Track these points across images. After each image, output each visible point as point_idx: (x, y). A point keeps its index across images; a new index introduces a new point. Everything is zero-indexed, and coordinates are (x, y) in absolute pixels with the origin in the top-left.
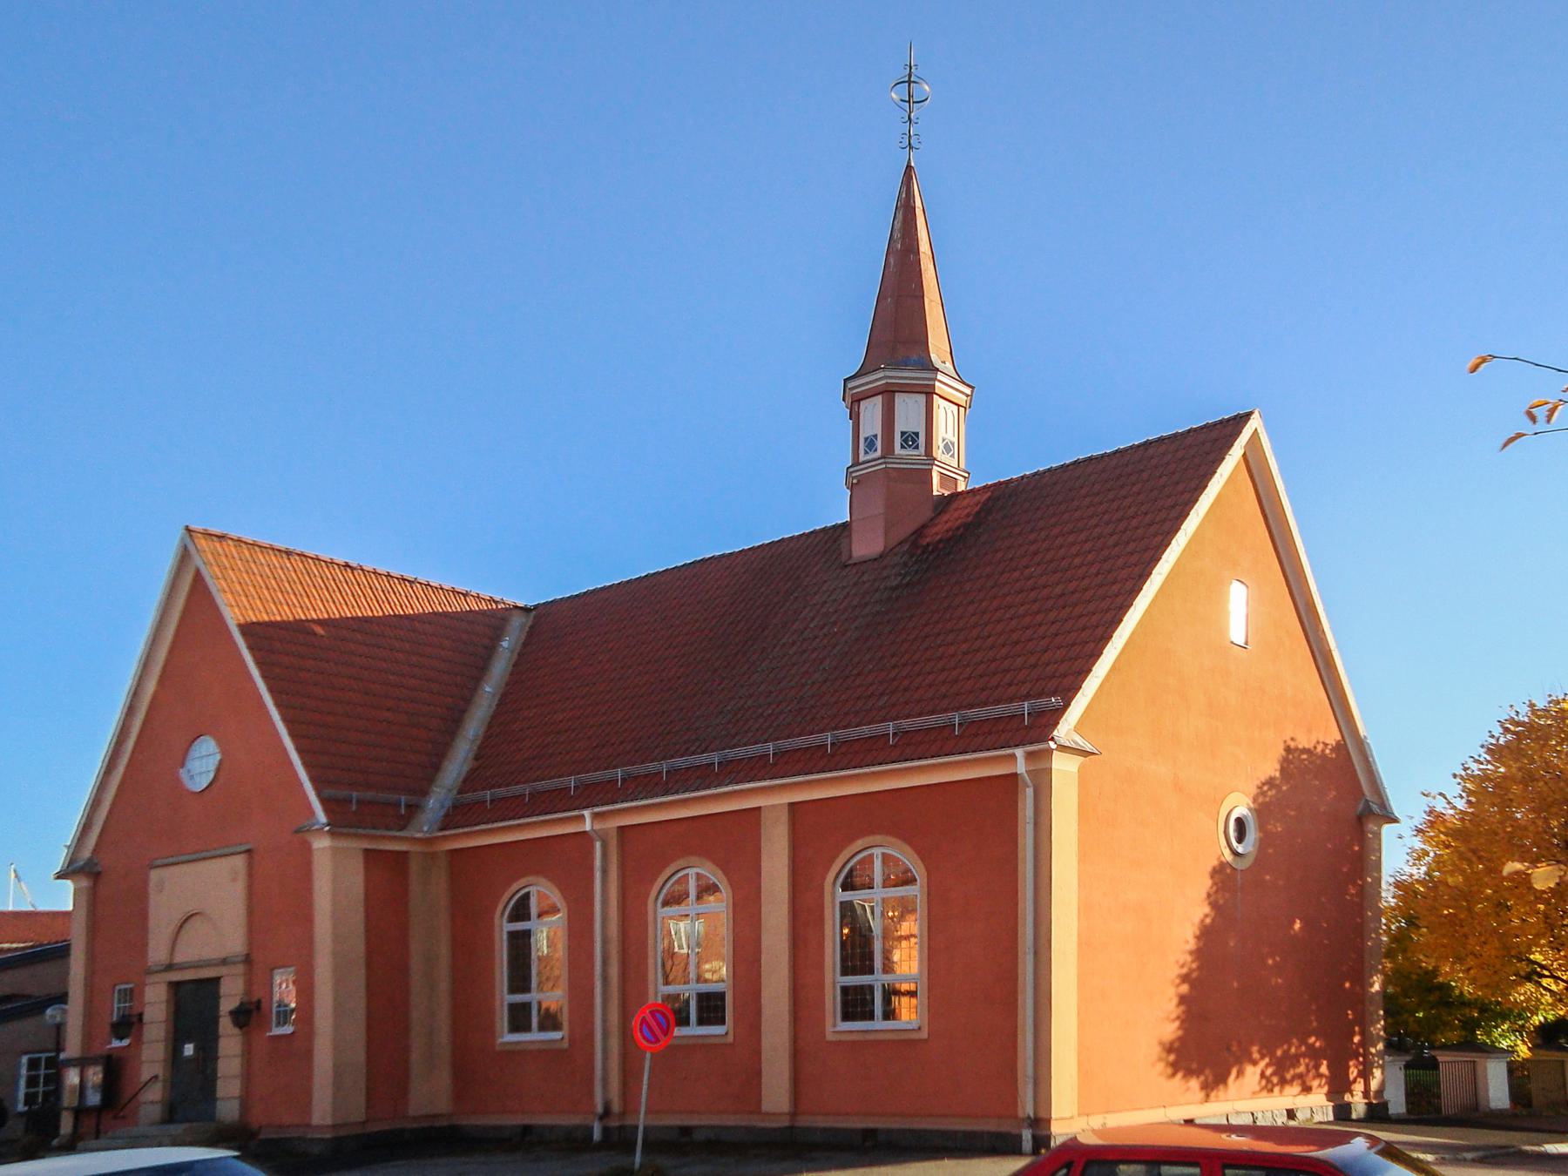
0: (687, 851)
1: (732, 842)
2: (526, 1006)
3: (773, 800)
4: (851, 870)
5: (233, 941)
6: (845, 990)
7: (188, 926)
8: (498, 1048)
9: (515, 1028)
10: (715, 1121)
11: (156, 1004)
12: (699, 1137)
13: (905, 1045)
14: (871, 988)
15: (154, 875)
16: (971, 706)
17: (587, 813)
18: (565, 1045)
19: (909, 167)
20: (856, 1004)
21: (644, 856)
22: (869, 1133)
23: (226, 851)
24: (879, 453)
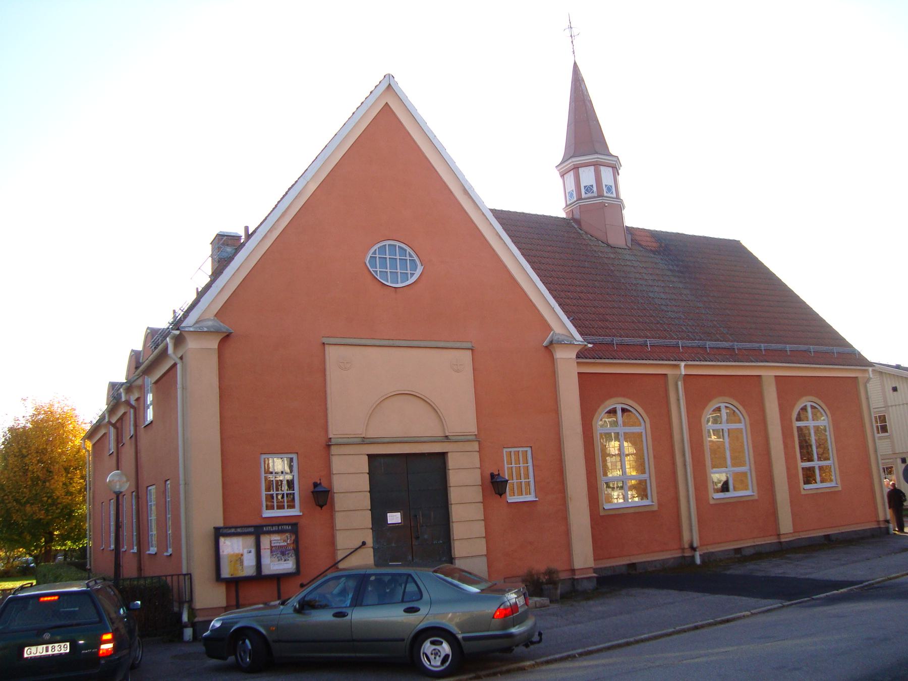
0: (721, 393)
1: (747, 392)
2: (812, 469)
3: (769, 372)
4: (629, 411)
5: (463, 418)
6: (814, 467)
7: (422, 403)
8: (602, 513)
9: (807, 482)
10: (749, 543)
11: (351, 480)
12: (747, 553)
13: (831, 495)
14: (814, 467)
15: (333, 354)
16: (742, 342)
17: (683, 364)
18: (655, 508)
19: (575, 64)
20: (809, 475)
21: (700, 392)
22: (827, 537)
23: (458, 345)
24: (595, 194)
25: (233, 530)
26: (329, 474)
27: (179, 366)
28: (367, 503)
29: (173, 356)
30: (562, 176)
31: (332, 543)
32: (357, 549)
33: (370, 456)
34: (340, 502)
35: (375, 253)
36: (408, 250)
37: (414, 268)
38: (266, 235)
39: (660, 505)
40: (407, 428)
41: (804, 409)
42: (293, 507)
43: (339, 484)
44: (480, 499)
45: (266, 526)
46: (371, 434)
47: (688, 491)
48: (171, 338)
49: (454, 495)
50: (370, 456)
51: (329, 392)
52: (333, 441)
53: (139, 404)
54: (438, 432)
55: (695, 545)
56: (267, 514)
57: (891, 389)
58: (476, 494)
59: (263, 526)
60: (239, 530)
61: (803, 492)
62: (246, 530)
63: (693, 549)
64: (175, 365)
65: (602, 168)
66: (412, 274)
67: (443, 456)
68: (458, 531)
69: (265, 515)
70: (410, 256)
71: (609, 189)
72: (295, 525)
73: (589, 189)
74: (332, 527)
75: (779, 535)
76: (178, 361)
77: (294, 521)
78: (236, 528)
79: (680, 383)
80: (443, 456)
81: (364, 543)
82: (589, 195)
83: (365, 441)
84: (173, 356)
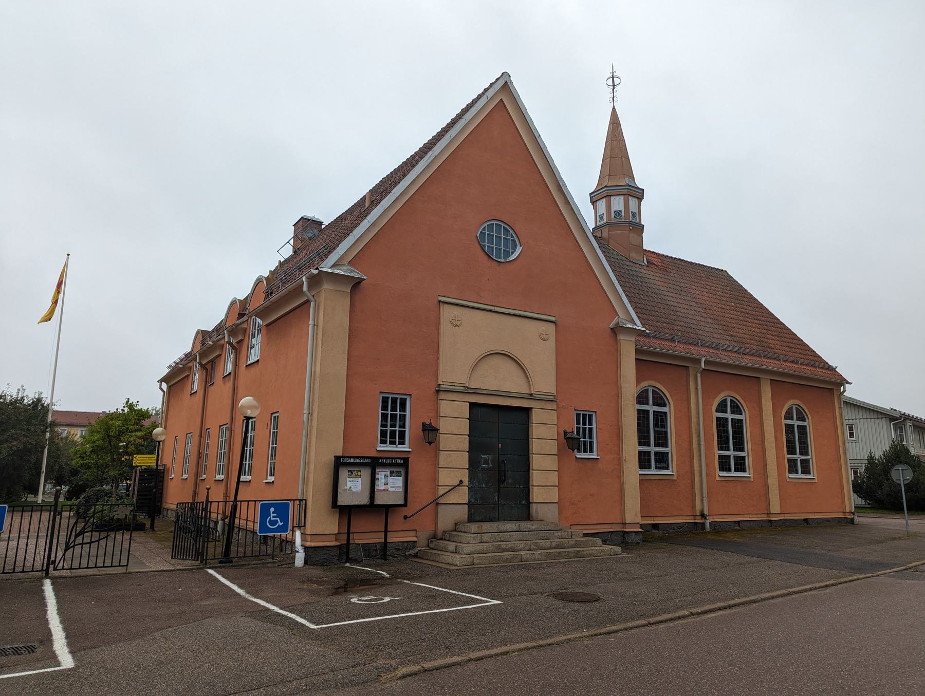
2: (795, 461)
25: (352, 460)
26: (437, 415)
27: (312, 304)
28: (466, 446)
29: (308, 293)
30: (593, 202)
31: (435, 480)
32: (455, 487)
33: (472, 405)
34: (444, 441)
35: (484, 229)
36: (511, 231)
37: (514, 247)
38: (397, 199)
39: (678, 476)
40: (503, 382)
41: (791, 409)
42: (403, 443)
43: (444, 426)
44: (555, 451)
45: (381, 458)
46: (474, 384)
47: (701, 466)
48: (307, 278)
49: (535, 446)
50: (472, 405)
51: (441, 343)
52: (443, 387)
53: (241, 347)
54: (524, 390)
55: (706, 512)
56: (381, 448)
57: (395, 388)
58: (553, 447)
59: (378, 458)
60: (357, 460)
61: (788, 480)
62: (363, 461)
63: (703, 516)
64: (308, 301)
65: (630, 198)
66: (512, 253)
67: (527, 410)
68: (536, 478)
69: (379, 449)
70: (512, 236)
71: (634, 215)
72: (406, 460)
73: (618, 213)
74: (436, 465)
75: (769, 514)
76: (312, 298)
77: (404, 456)
78: (355, 458)
79: (699, 375)
80: (527, 410)
81: (461, 482)
82: (602, 222)
83: (476, 392)
84: (308, 293)
